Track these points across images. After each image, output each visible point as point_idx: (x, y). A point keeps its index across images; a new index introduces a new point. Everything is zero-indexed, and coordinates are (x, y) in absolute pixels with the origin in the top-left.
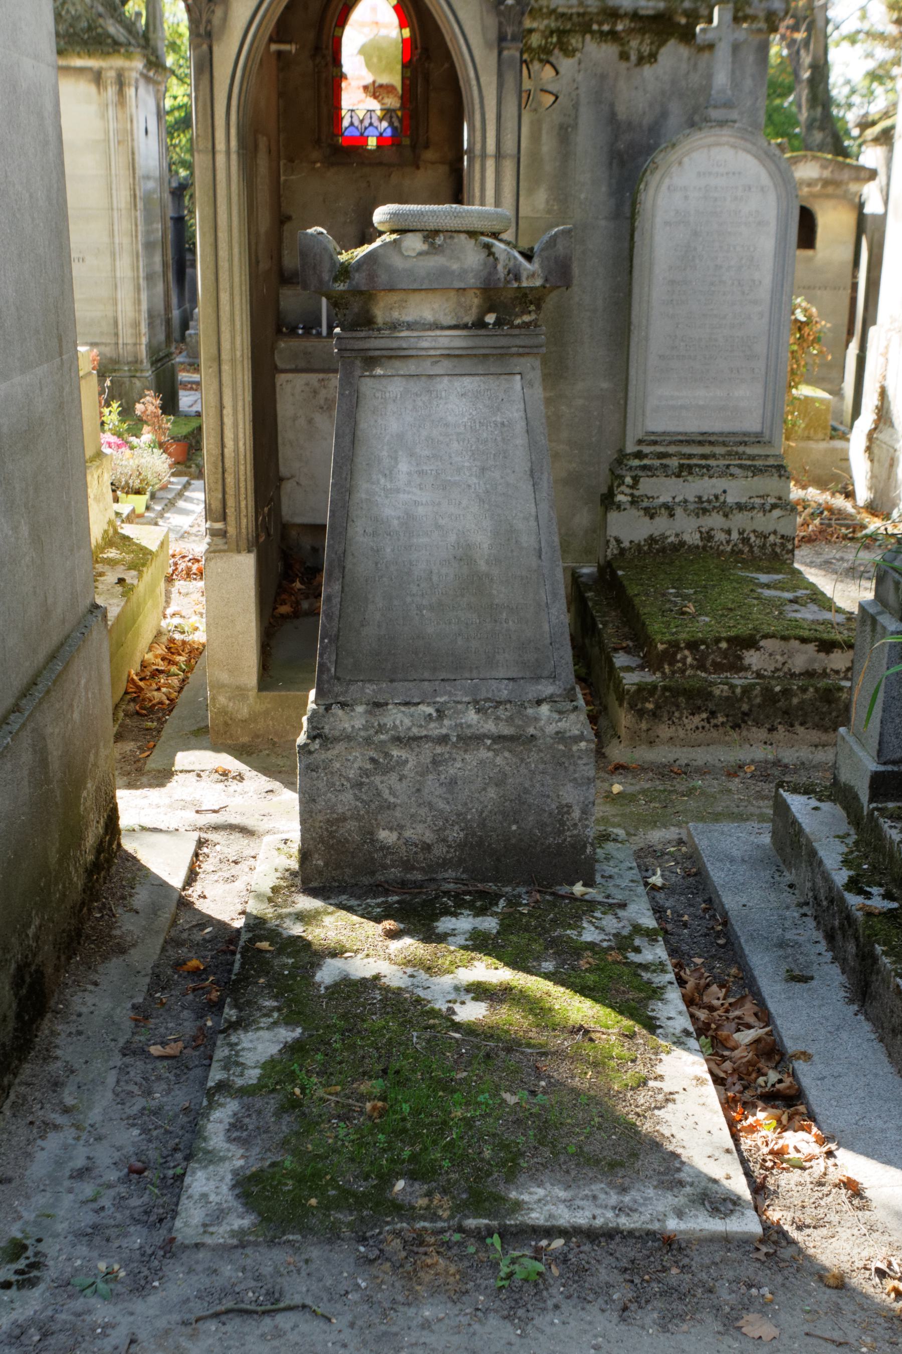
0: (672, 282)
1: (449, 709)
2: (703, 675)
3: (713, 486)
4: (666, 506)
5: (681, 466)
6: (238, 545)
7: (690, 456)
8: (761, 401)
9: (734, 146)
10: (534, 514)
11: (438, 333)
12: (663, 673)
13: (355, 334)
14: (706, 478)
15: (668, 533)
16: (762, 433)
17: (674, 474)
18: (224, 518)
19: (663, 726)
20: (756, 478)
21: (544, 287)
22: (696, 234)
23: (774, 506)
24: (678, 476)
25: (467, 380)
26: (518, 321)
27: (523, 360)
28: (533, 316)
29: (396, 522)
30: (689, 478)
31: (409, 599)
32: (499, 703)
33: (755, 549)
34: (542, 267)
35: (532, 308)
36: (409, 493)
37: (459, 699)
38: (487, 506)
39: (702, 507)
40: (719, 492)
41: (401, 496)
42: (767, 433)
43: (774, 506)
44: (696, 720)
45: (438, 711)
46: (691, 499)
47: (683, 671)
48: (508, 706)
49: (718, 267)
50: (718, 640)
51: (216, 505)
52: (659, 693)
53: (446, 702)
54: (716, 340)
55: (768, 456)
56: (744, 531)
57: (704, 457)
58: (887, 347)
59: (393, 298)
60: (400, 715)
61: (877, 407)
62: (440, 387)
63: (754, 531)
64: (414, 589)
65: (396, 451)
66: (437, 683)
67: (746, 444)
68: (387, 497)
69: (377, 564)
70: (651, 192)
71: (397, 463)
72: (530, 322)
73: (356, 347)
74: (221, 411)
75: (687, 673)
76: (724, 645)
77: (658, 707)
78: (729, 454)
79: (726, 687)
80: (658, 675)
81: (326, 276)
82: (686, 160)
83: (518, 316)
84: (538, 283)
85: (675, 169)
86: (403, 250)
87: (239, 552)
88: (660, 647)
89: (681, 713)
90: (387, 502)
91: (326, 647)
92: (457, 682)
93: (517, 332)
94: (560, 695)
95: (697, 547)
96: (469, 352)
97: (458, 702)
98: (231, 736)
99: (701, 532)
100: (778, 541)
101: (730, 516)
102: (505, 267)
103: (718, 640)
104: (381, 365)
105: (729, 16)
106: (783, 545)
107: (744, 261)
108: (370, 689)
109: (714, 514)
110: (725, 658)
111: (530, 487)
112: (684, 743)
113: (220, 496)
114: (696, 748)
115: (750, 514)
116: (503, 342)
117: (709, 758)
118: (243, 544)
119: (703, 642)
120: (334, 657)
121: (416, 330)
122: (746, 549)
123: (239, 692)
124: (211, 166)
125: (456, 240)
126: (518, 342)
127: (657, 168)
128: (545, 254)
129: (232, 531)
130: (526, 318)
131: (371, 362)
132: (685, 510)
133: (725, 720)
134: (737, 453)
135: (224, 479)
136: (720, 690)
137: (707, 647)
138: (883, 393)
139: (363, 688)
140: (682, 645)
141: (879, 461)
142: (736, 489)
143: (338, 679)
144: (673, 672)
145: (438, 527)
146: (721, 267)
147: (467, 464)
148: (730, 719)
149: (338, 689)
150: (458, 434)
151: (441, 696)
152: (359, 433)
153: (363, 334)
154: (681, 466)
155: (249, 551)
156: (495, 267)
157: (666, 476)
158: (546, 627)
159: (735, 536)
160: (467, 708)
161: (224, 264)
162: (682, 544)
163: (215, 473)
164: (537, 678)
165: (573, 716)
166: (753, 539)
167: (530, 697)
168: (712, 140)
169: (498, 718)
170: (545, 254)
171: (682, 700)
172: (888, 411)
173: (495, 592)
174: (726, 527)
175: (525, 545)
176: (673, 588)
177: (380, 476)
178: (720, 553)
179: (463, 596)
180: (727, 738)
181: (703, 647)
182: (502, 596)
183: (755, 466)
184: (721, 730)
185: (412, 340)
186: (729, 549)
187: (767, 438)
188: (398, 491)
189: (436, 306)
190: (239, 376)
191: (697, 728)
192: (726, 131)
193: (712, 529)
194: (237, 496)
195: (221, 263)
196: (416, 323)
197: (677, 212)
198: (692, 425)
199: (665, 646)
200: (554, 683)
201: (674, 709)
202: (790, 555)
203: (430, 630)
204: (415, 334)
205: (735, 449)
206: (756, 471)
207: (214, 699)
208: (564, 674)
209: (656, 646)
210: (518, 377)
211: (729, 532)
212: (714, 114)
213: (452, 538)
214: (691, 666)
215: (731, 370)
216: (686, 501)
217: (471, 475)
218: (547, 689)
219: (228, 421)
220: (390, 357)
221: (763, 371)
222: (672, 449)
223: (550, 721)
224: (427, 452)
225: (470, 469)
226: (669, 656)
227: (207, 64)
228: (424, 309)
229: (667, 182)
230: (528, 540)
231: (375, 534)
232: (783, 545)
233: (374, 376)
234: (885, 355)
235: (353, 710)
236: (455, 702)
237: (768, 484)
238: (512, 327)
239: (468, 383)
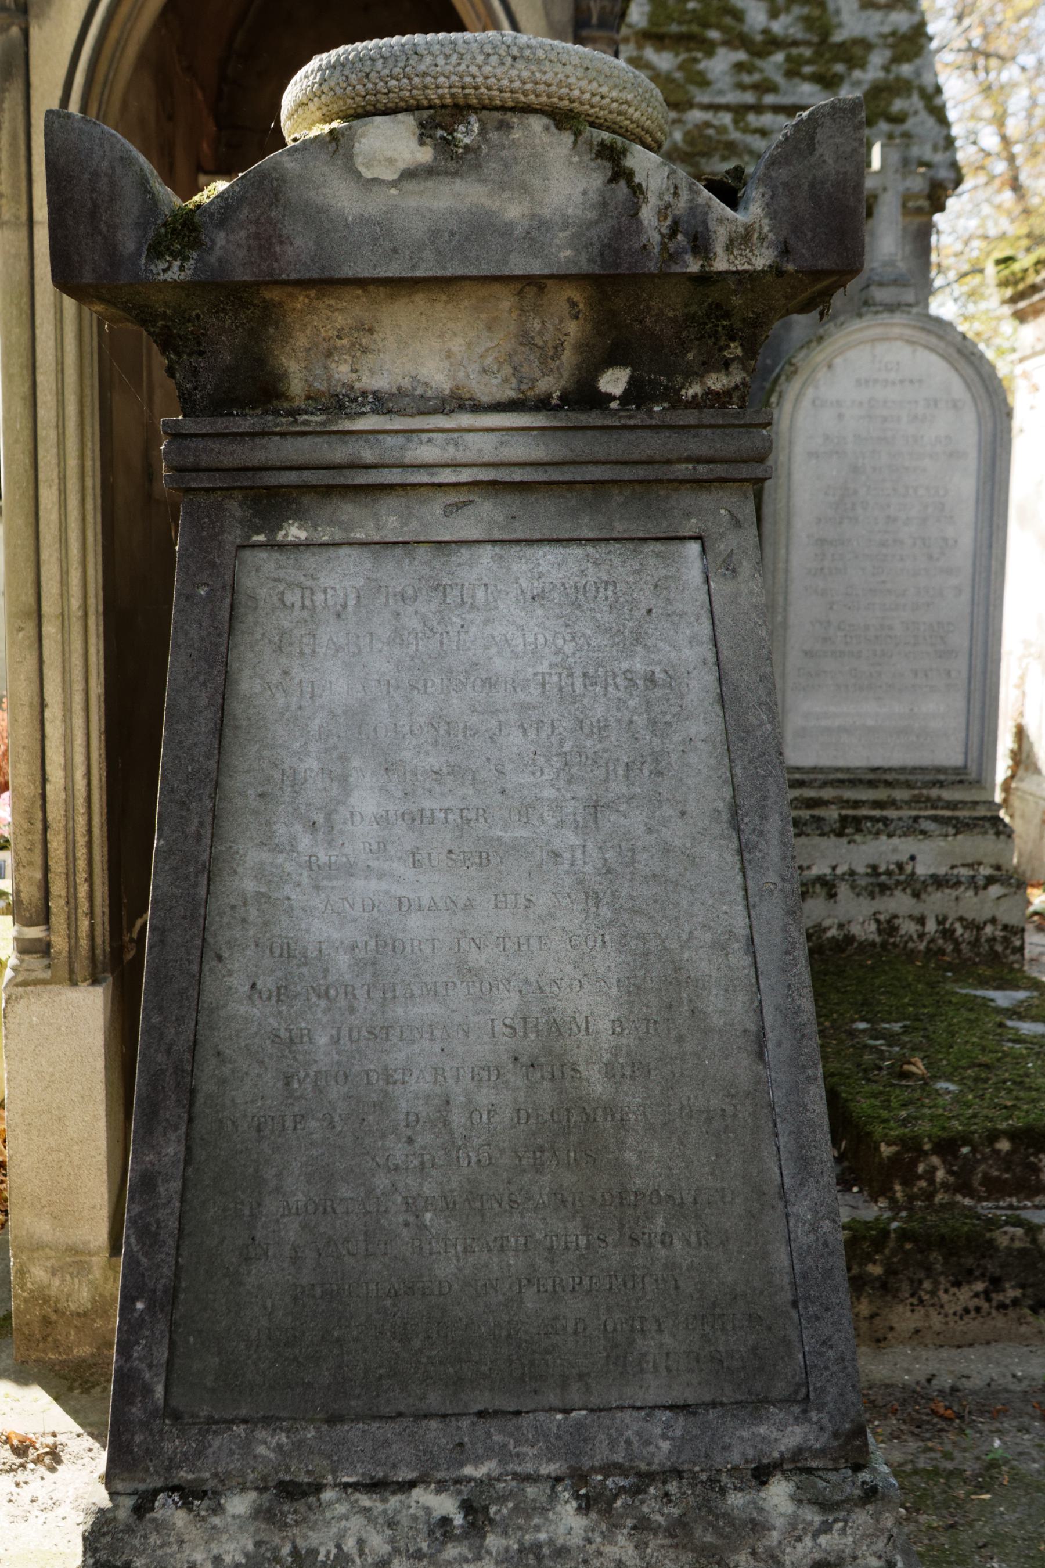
0: (822, 542)
1: (502, 1499)
2: (967, 1202)
3: (895, 850)
4: (821, 880)
5: (843, 819)
6: (71, 972)
7: (857, 804)
8: (963, 720)
9: (910, 342)
10: (741, 931)
11: (466, 420)
12: (893, 1200)
13: (220, 425)
14: (884, 838)
15: (826, 923)
16: (965, 767)
17: (833, 831)
18: (44, 917)
19: (900, 1308)
20: (960, 837)
21: (776, 271)
22: (855, 469)
23: (990, 880)
24: (840, 834)
25: (547, 557)
26: (694, 390)
27: (706, 499)
28: (737, 376)
29: (343, 960)
30: (858, 838)
31: (382, 1182)
32: (648, 1478)
33: (964, 946)
34: (772, 213)
35: (735, 350)
36: (381, 876)
37: (529, 1468)
38: (606, 912)
39: (879, 882)
40: (904, 858)
41: (359, 884)
42: (973, 768)
43: (990, 880)
44: (964, 1295)
45: (467, 1507)
46: (861, 869)
47: (929, 1196)
48: (673, 1487)
49: (891, 519)
50: (993, 1136)
51: (31, 893)
52: (892, 1244)
53: (490, 1480)
54: (891, 628)
55: (976, 803)
56: (945, 919)
57: (878, 804)
58: (1022, 678)
59: (336, 316)
60: (356, 1523)
61: (1012, 751)
62: (469, 575)
63: (961, 919)
64: (399, 1152)
65: (344, 758)
66: (465, 1423)
67: (941, 784)
68: (317, 888)
69: (288, 1081)
70: (787, 406)
71: (346, 789)
72: (728, 393)
73: (226, 462)
74: (42, 712)
75: (938, 1198)
76: (1004, 1145)
77: (891, 1271)
78: (916, 800)
79: (1019, 1231)
80: (883, 1203)
81: (128, 242)
82: (838, 361)
83: (693, 374)
84: (762, 259)
85: (822, 374)
86: (359, 162)
87: (73, 983)
88: (886, 1150)
89: (936, 1284)
90: (317, 901)
91: (141, 1323)
92: (526, 1421)
93: (690, 417)
94: (822, 1452)
95: (873, 944)
96: (555, 475)
97: (528, 1478)
98: (57, 1345)
99: (878, 921)
100: (999, 934)
101: (923, 896)
102: (662, 213)
103: (993, 1136)
104: (300, 516)
105: (895, 157)
106: (1006, 940)
107: (930, 510)
108: (267, 1445)
109: (898, 893)
110: (1007, 1170)
111: (731, 858)
112: (944, 1341)
113: (38, 875)
114: (966, 1351)
115: (955, 893)
116: (652, 445)
117: (992, 1371)
118: (82, 967)
119: (966, 1140)
120: (162, 1354)
121: (401, 412)
122: (949, 947)
123: (74, 1258)
124: (25, 251)
125: (516, 135)
126: (695, 446)
127: (795, 372)
128: (783, 174)
129: (59, 943)
130: (717, 382)
131: (272, 501)
132: (853, 887)
133: (1017, 1293)
134: (928, 799)
135: (45, 842)
136: (1008, 1237)
137: (974, 1150)
138: (1020, 733)
139: (247, 1445)
140: (927, 1147)
141: (1023, 816)
142: (930, 855)
143: (176, 1417)
144: (911, 1198)
145: (466, 971)
146: (895, 520)
147: (548, 793)
148: (1029, 1291)
149: (172, 1446)
150: (525, 707)
151: (478, 1461)
152: (236, 707)
153: (244, 425)
154: (843, 819)
155: (95, 981)
156: (634, 214)
157: (822, 835)
158: (781, 1258)
159: (931, 926)
160: (553, 1497)
161: (47, 434)
162: (849, 939)
163: (28, 832)
164: (756, 1405)
165: (862, 1517)
166: (959, 931)
167: (735, 1458)
168: (878, 331)
169: (643, 1526)
170: (783, 174)
171: (936, 1257)
172: (1030, 755)
173: (631, 1157)
174: (916, 913)
175: (717, 1021)
176: (863, 1019)
177: (298, 828)
178: (911, 955)
179: (539, 1169)
180: (1023, 1329)
181: (965, 1150)
182: (650, 1167)
183: (957, 818)
184: (1012, 1314)
185: (389, 440)
186: (922, 946)
187: (973, 776)
188: (349, 870)
189: (457, 345)
190: (77, 645)
191: (967, 1311)
192: (898, 318)
193: (896, 917)
194: (70, 875)
195: (41, 433)
196: (401, 392)
197: (827, 437)
198: (858, 756)
199: (894, 1149)
200: (803, 1417)
201: (922, 1275)
202: (1017, 956)
203: (445, 1269)
204: (399, 423)
205: (925, 792)
206: (961, 826)
207: (22, 1272)
208: (833, 1391)
209: (877, 1149)
210: (694, 547)
211: (921, 921)
212: (880, 294)
213: (508, 1003)
214: (945, 1185)
215: (916, 673)
216: (852, 873)
217: (561, 824)
218: (788, 1435)
219: (54, 731)
220: (328, 491)
221: (965, 675)
222: (827, 793)
223: (795, 1532)
224: (433, 761)
225: (557, 806)
226: (902, 1168)
227: (20, 62)
228: (427, 352)
229: (810, 392)
230: (725, 1008)
231: (281, 993)
232: (1006, 940)
233: (281, 546)
234: (1020, 685)
235: (218, 1509)
236: (516, 1476)
237: (979, 846)
238: (677, 403)
239: (555, 565)
